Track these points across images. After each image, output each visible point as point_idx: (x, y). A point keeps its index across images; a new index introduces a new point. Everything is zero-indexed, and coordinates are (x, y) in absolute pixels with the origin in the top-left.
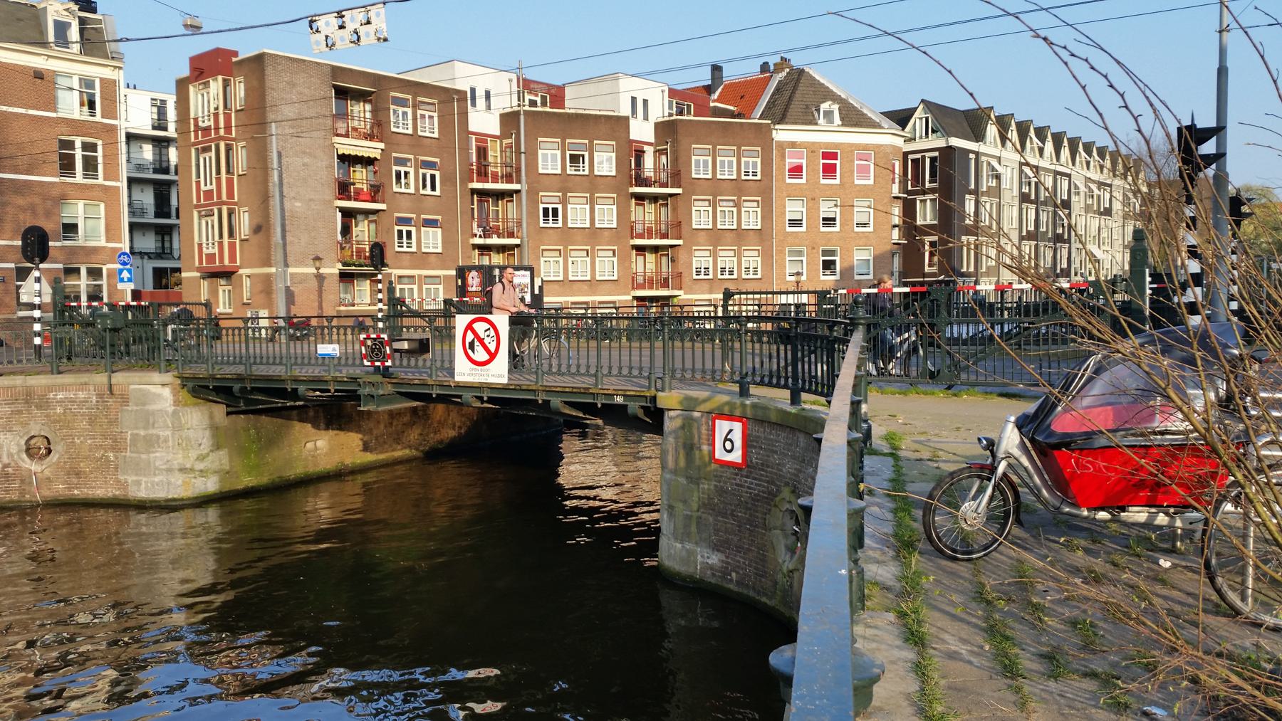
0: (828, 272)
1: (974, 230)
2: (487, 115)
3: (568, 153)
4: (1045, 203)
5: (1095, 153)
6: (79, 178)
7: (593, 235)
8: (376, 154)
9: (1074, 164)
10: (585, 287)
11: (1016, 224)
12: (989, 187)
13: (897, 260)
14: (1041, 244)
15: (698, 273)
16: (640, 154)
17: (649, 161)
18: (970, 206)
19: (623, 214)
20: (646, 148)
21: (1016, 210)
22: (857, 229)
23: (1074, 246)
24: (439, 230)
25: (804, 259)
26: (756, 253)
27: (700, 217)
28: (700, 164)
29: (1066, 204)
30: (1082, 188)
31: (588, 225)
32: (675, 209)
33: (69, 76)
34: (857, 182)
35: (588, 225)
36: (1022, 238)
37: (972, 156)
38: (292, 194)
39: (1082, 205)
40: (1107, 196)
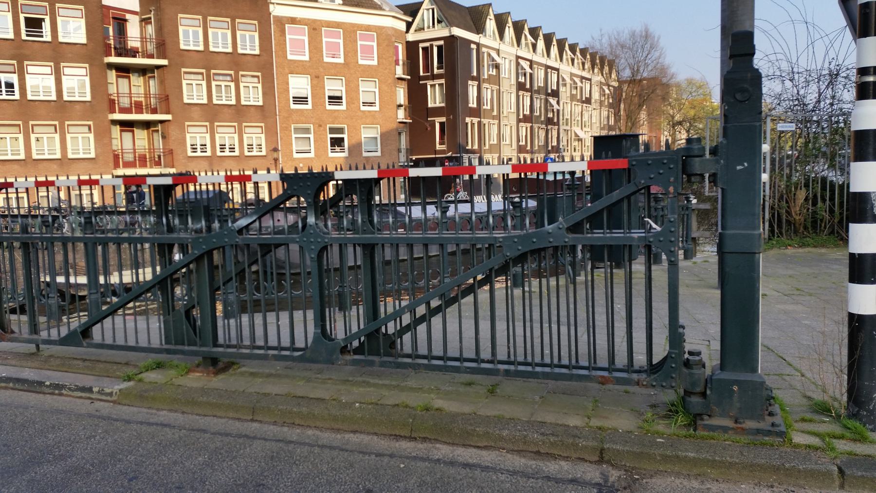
0: (337, 149)
1: (476, 112)
3: (22, 17)
4: (538, 92)
5: (578, 53)
7: (60, 110)
9: (561, 60)
11: (514, 109)
12: (489, 76)
13: (403, 137)
14: (536, 126)
15: (194, 150)
16: (121, 23)
17: (133, 29)
18: (473, 92)
19: (98, 85)
21: (514, 96)
22: (363, 108)
23: (562, 128)
25: (311, 136)
26: (259, 130)
27: (193, 90)
28: (189, 34)
29: (555, 94)
30: (568, 81)
32: (162, 82)
34: (361, 62)
35: (54, 97)
36: (519, 121)
37: (473, 46)
39: (568, 95)
40: (588, 86)
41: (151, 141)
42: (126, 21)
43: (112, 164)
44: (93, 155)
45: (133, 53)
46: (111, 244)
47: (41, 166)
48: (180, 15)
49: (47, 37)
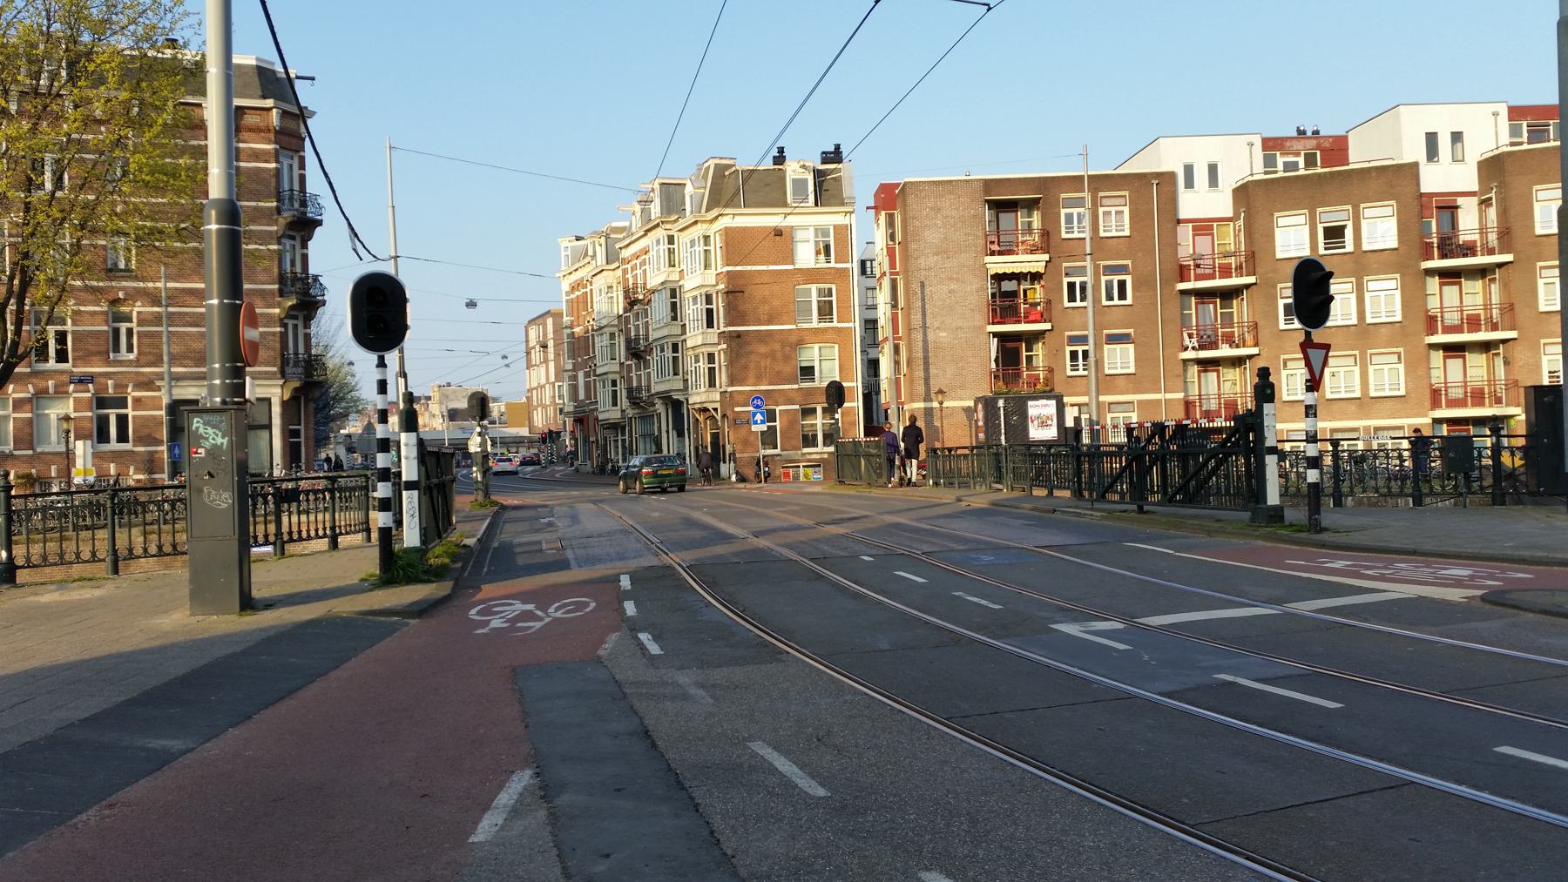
2: (1214, 195)
6: (52, 364)
8: (1040, 268)
10: (1352, 407)
17: (1469, 222)
19: (1413, 298)
20: (1460, 201)
24: (1131, 347)
31: (1354, 321)
32: (1505, 286)
33: (805, 228)
35: (1354, 321)
38: (936, 324)
41: (1491, 369)
42: (1457, 207)
43: (1428, 403)
44: (1402, 392)
45: (1469, 250)
46: (957, 434)
47: (1335, 407)
48: (1536, 187)
49: (1349, 247)
